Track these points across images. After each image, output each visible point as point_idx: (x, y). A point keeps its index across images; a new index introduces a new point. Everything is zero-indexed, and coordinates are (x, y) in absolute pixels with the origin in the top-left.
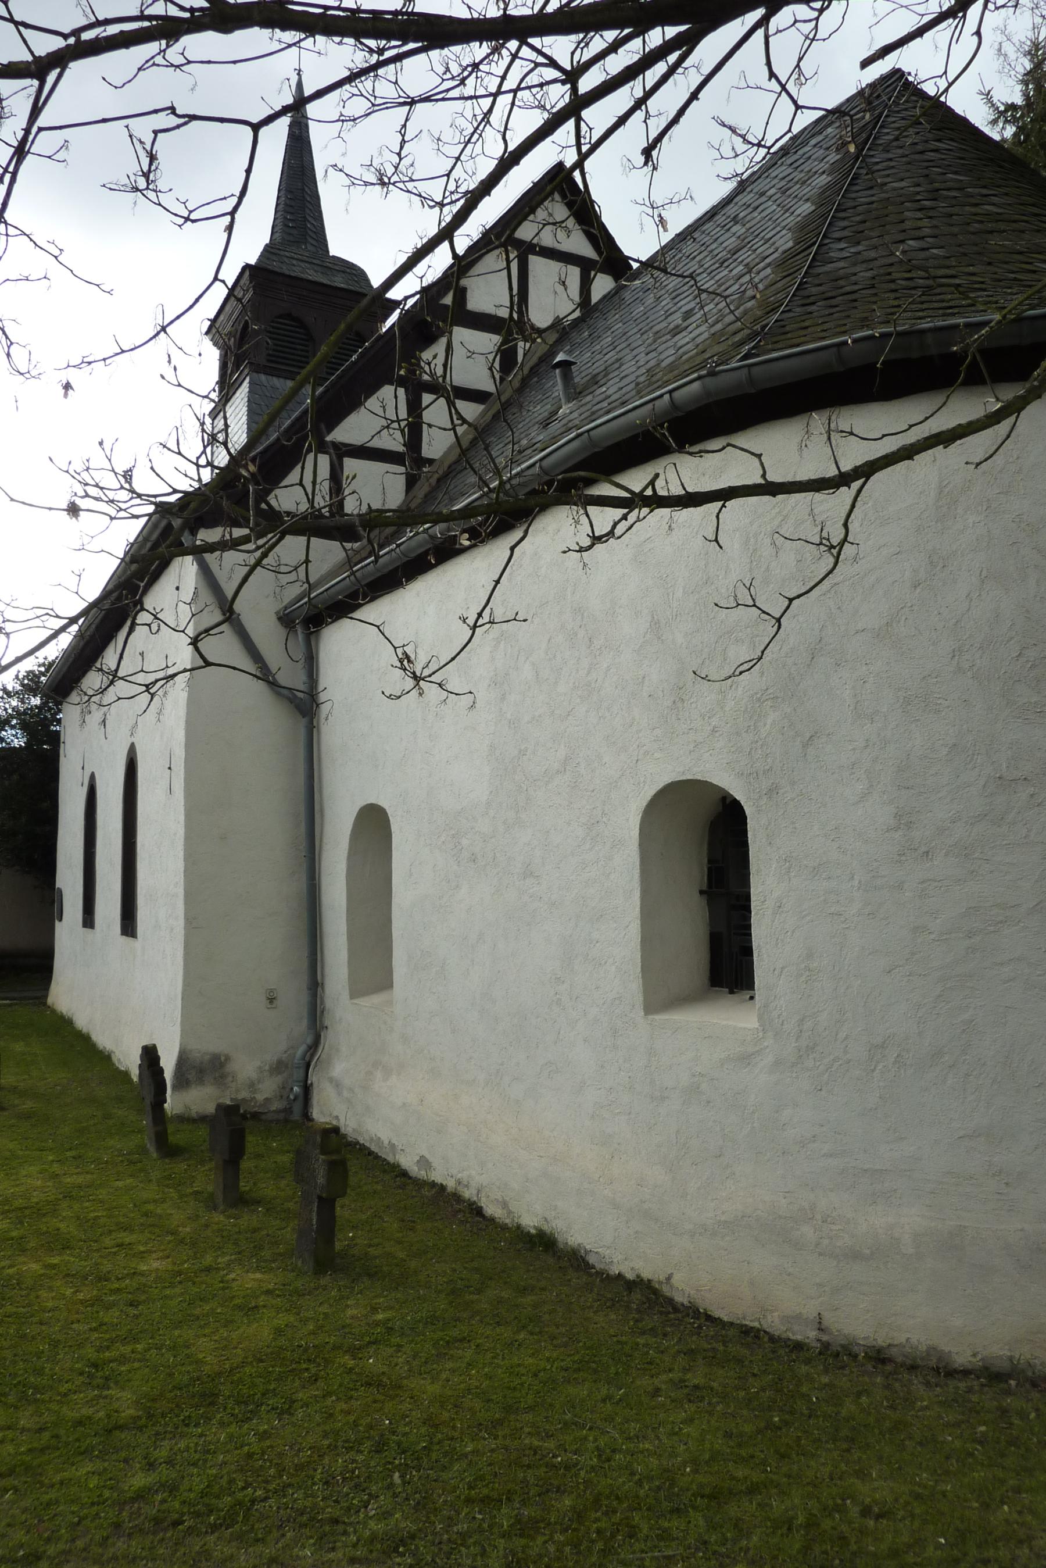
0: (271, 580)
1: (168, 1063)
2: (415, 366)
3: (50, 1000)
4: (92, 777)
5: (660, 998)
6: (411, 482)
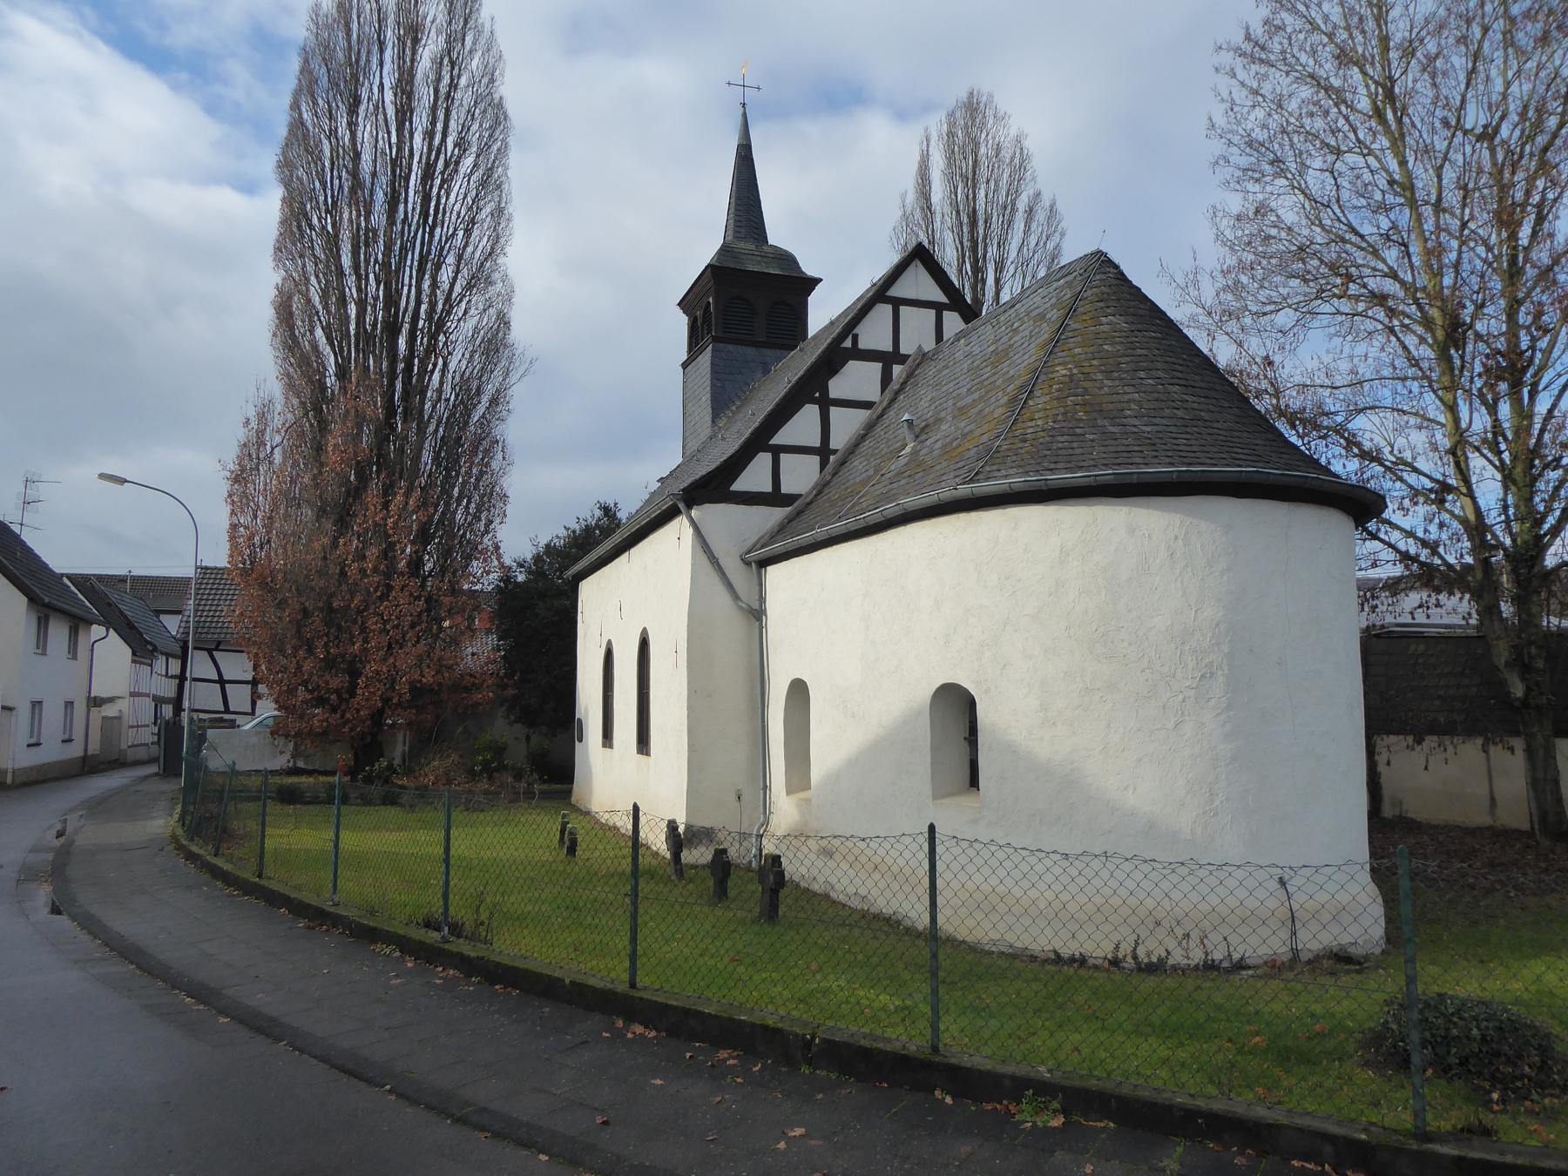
0: (734, 525)
1: (681, 829)
2: (825, 390)
3: (573, 799)
4: (609, 642)
5: (939, 793)
6: (824, 464)
